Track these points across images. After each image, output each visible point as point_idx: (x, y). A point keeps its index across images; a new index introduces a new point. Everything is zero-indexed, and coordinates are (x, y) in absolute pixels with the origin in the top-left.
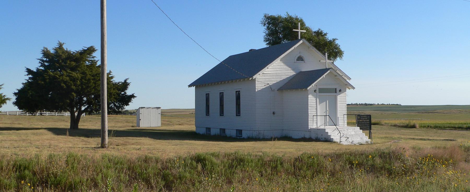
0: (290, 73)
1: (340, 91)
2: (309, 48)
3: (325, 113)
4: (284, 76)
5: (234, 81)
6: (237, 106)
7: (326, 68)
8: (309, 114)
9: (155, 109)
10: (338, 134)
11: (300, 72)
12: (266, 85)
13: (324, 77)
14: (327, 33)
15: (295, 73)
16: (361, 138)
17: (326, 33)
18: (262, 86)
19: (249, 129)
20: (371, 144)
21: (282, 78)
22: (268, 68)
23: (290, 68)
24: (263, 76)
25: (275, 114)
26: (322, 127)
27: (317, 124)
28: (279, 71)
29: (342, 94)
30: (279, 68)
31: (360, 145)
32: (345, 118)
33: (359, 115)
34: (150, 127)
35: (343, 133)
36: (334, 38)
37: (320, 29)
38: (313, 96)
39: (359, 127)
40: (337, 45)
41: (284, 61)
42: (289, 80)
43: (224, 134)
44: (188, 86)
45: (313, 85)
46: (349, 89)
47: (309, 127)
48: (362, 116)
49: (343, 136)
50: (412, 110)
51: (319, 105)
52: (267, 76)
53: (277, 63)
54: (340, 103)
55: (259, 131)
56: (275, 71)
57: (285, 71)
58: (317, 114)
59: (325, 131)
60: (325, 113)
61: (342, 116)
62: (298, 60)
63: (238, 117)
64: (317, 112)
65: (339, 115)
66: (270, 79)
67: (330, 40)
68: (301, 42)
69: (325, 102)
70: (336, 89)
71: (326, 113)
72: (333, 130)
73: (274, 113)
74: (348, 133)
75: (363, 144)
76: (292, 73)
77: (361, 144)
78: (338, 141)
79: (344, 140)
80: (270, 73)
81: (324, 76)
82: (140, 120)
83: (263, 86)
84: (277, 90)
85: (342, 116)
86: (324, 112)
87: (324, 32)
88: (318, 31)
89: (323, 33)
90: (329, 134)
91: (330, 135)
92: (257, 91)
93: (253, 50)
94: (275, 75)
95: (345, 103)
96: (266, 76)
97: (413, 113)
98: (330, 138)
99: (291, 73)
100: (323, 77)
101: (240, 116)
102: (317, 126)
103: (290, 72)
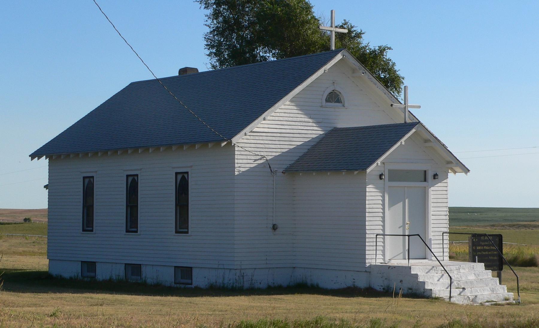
0: (310, 132)
1: (434, 178)
2: (354, 71)
3: (402, 228)
5: (174, 148)
6: (178, 208)
7: (405, 123)
8: (367, 232)
10: (438, 281)
11: (332, 130)
12: (258, 160)
13: (403, 143)
14: (363, 32)
15: (322, 133)
16: (493, 290)
17: (361, 31)
19: (216, 266)
20: (516, 304)
22: (264, 119)
24: (252, 137)
25: (277, 230)
26: (404, 263)
27: (384, 255)
29: (439, 184)
31: (492, 305)
32: (445, 242)
33: (474, 235)
36: (383, 44)
37: (347, 21)
39: (483, 264)
40: (388, 63)
41: (297, 102)
43: (140, 277)
44: (30, 156)
45: (379, 163)
46: (455, 172)
47: (367, 261)
50: (473, 220)
51: (389, 210)
53: (283, 107)
54: (435, 205)
57: (300, 128)
58: (384, 230)
59: (411, 272)
61: (437, 238)
62: (327, 101)
63: (182, 238)
64: (384, 226)
65: (432, 234)
66: (267, 146)
67: (373, 48)
68: (339, 57)
70: (425, 171)
71: (404, 230)
72: (427, 271)
73: (275, 227)
74: (461, 277)
75: (499, 305)
77: (496, 305)
78: (445, 294)
79: (456, 295)
80: (266, 130)
81: (403, 140)
83: (251, 161)
84: (282, 172)
85: (437, 238)
86: (399, 228)
87: (357, 29)
89: (355, 31)
90: (421, 279)
92: (238, 173)
93: (189, 73)
94: (279, 135)
95: (445, 205)
96: (257, 138)
97: (479, 227)
98: (424, 289)
99: (314, 132)
101: (187, 232)
102: (384, 259)
103: (312, 128)
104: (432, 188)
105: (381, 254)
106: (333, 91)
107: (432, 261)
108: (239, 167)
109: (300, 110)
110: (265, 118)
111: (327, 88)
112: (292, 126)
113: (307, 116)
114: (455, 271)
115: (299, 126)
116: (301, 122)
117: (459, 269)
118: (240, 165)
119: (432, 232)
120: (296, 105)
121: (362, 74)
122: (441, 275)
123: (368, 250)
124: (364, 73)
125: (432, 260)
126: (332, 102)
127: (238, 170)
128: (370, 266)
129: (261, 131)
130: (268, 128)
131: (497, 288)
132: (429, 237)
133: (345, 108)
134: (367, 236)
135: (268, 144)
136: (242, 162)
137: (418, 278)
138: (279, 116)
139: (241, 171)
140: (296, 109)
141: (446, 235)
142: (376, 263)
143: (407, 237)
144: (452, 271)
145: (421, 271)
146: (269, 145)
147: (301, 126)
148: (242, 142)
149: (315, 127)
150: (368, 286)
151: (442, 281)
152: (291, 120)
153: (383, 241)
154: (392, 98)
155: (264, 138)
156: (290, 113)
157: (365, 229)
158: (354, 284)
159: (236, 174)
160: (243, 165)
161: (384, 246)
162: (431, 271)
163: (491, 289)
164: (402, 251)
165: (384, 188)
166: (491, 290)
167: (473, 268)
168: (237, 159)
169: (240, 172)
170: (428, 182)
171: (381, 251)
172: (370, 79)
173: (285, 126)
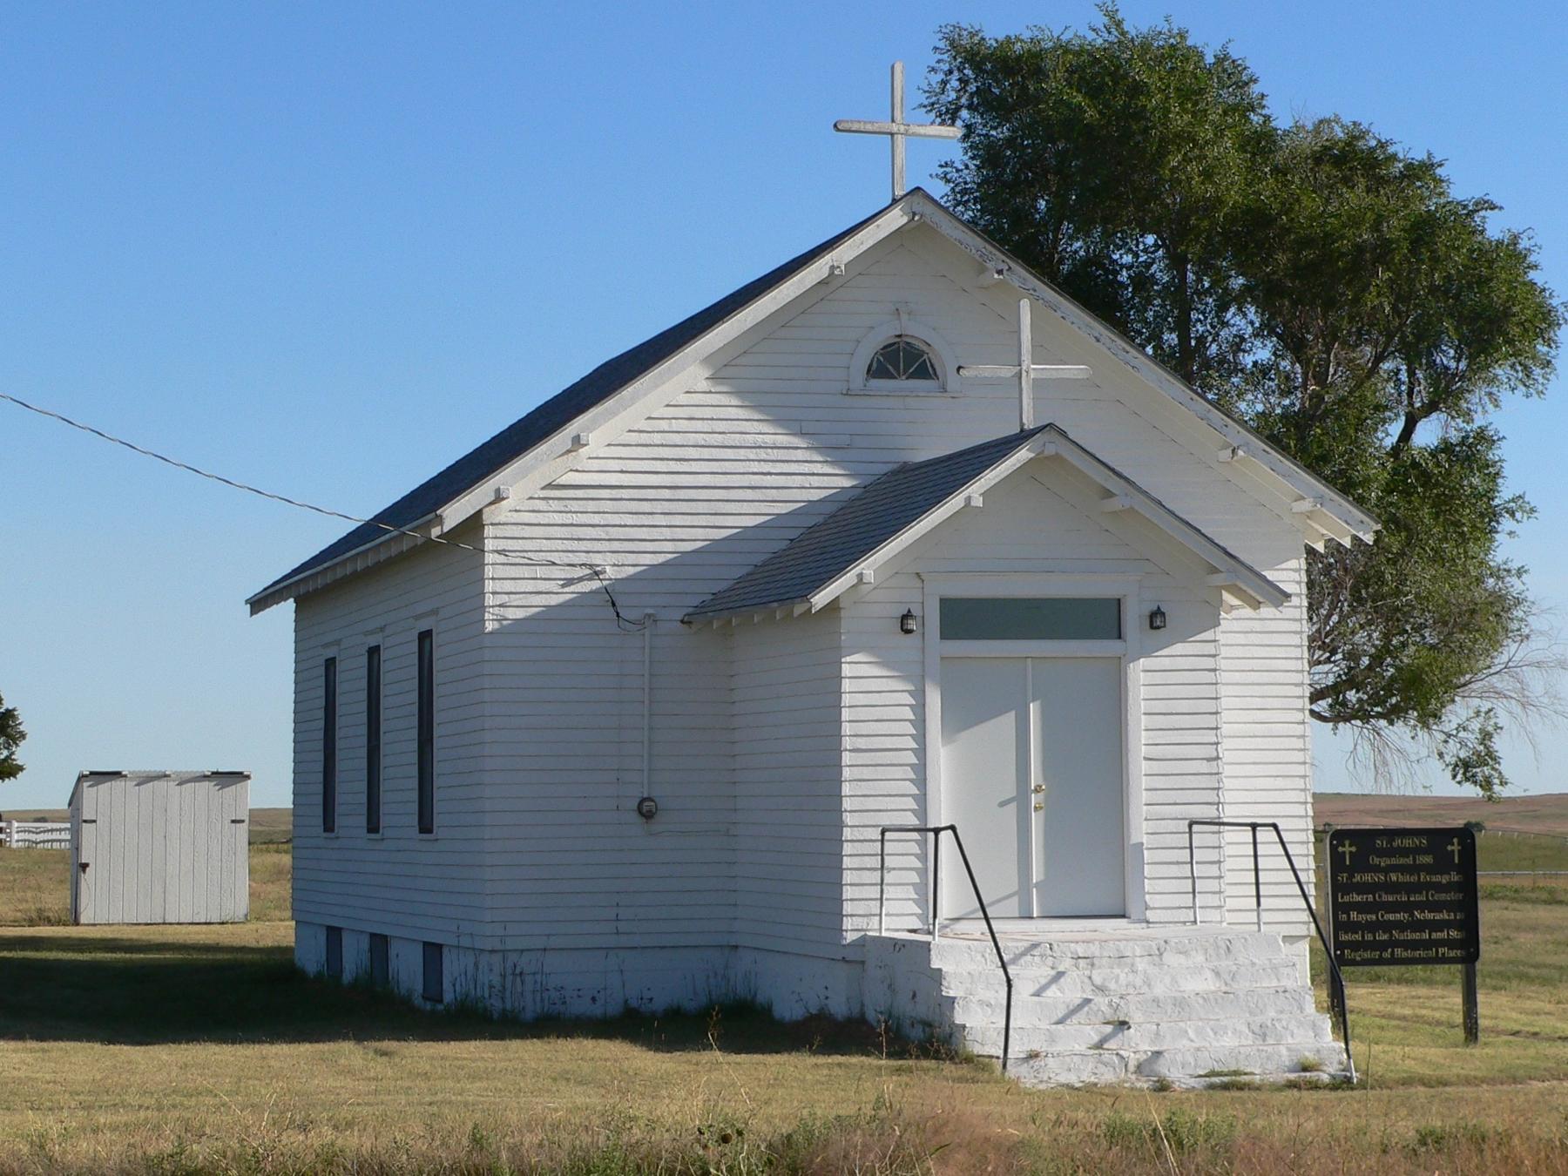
0: (798, 481)
3: (1013, 806)
4: (745, 508)
8: (848, 819)
9: (206, 784)
10: (1037, 994)
11: (894, 473)
12: (580, 579)
13: (978, 502)
15: (847, 483)
16: (1262, 1034)
18: (542, 586)
21: (730, 521)
23: (796, 441)
24: (555, 505)
28: (695, 467)
29: (1179, 648)
30: (700, 439)
31: (1212, 1087)
34: (161, 921)
35: (1098, 980)
42: (794, 534)
47: (848, 923)
49: (1079, 1007)
52: (591, 506)
55: (513, 957)
56: (659, 466)
57: (755, 467)
58: (922, 812)
60: (1013, 806)
69: (1013, 714)
70: (1119, 600)
76: (825, 481)
82: (84, 866)
83: (552, 586)
84: (682, 622)
86: (1002, 804)
88: (1349, 144)
91: (952, 994)
92: (497, 625)
94: (667, 494)
96: (575, 506)
99: (815, 481)
100: (969, 499)
103: (806, 468)
104: (1142, 660)
106: (898, 340)
107: (1144, 925)
108: (500, 606)
110: (579, 436)
111: (873, 328)
112: (727, 463)
113: (784, 427)
114: (1138, 959)
115: (753, 460)
116: (760, 447)
117: (1161, 954)
118: (507, 600)
119: (1146, 819)
121: (996, 276)
122: (1053, 973)
123: (851, 885)
124: (1005, 272)
125: (1148, 922)
126: (895, 378)
128: (863, 942)
129: (593, 484)
130: (622, 472)
131: (1284, 1023)
132: (1132, 837)
134: (847, 833)
135: (620, 526)
137: (944, 983)
138: (667, 429)
140: (740, 404)
141: (1214, 833)
142: (880, 929)
143: (931, 835)
144: (1128, 961)
145: (979, 957)
146: (627, 529)
147: (759, 461)
149: (819, 465)
150: (856, 1011)
151: (1059, 994)
152: (716, 444)
155: (608, 506)
156: (712, 419)
157: (840, 812)
158: (826, 1005)
159: (487, 631)
160: (515, 600)
162: (1029, 958)
163: (1257, 1029)
165: (923, 662)
166: (1254, 1033)
167: (1228, 948)
168: (493, 579)
169: (505, 622)
170: (1125, 641)
172: (1031, 292)
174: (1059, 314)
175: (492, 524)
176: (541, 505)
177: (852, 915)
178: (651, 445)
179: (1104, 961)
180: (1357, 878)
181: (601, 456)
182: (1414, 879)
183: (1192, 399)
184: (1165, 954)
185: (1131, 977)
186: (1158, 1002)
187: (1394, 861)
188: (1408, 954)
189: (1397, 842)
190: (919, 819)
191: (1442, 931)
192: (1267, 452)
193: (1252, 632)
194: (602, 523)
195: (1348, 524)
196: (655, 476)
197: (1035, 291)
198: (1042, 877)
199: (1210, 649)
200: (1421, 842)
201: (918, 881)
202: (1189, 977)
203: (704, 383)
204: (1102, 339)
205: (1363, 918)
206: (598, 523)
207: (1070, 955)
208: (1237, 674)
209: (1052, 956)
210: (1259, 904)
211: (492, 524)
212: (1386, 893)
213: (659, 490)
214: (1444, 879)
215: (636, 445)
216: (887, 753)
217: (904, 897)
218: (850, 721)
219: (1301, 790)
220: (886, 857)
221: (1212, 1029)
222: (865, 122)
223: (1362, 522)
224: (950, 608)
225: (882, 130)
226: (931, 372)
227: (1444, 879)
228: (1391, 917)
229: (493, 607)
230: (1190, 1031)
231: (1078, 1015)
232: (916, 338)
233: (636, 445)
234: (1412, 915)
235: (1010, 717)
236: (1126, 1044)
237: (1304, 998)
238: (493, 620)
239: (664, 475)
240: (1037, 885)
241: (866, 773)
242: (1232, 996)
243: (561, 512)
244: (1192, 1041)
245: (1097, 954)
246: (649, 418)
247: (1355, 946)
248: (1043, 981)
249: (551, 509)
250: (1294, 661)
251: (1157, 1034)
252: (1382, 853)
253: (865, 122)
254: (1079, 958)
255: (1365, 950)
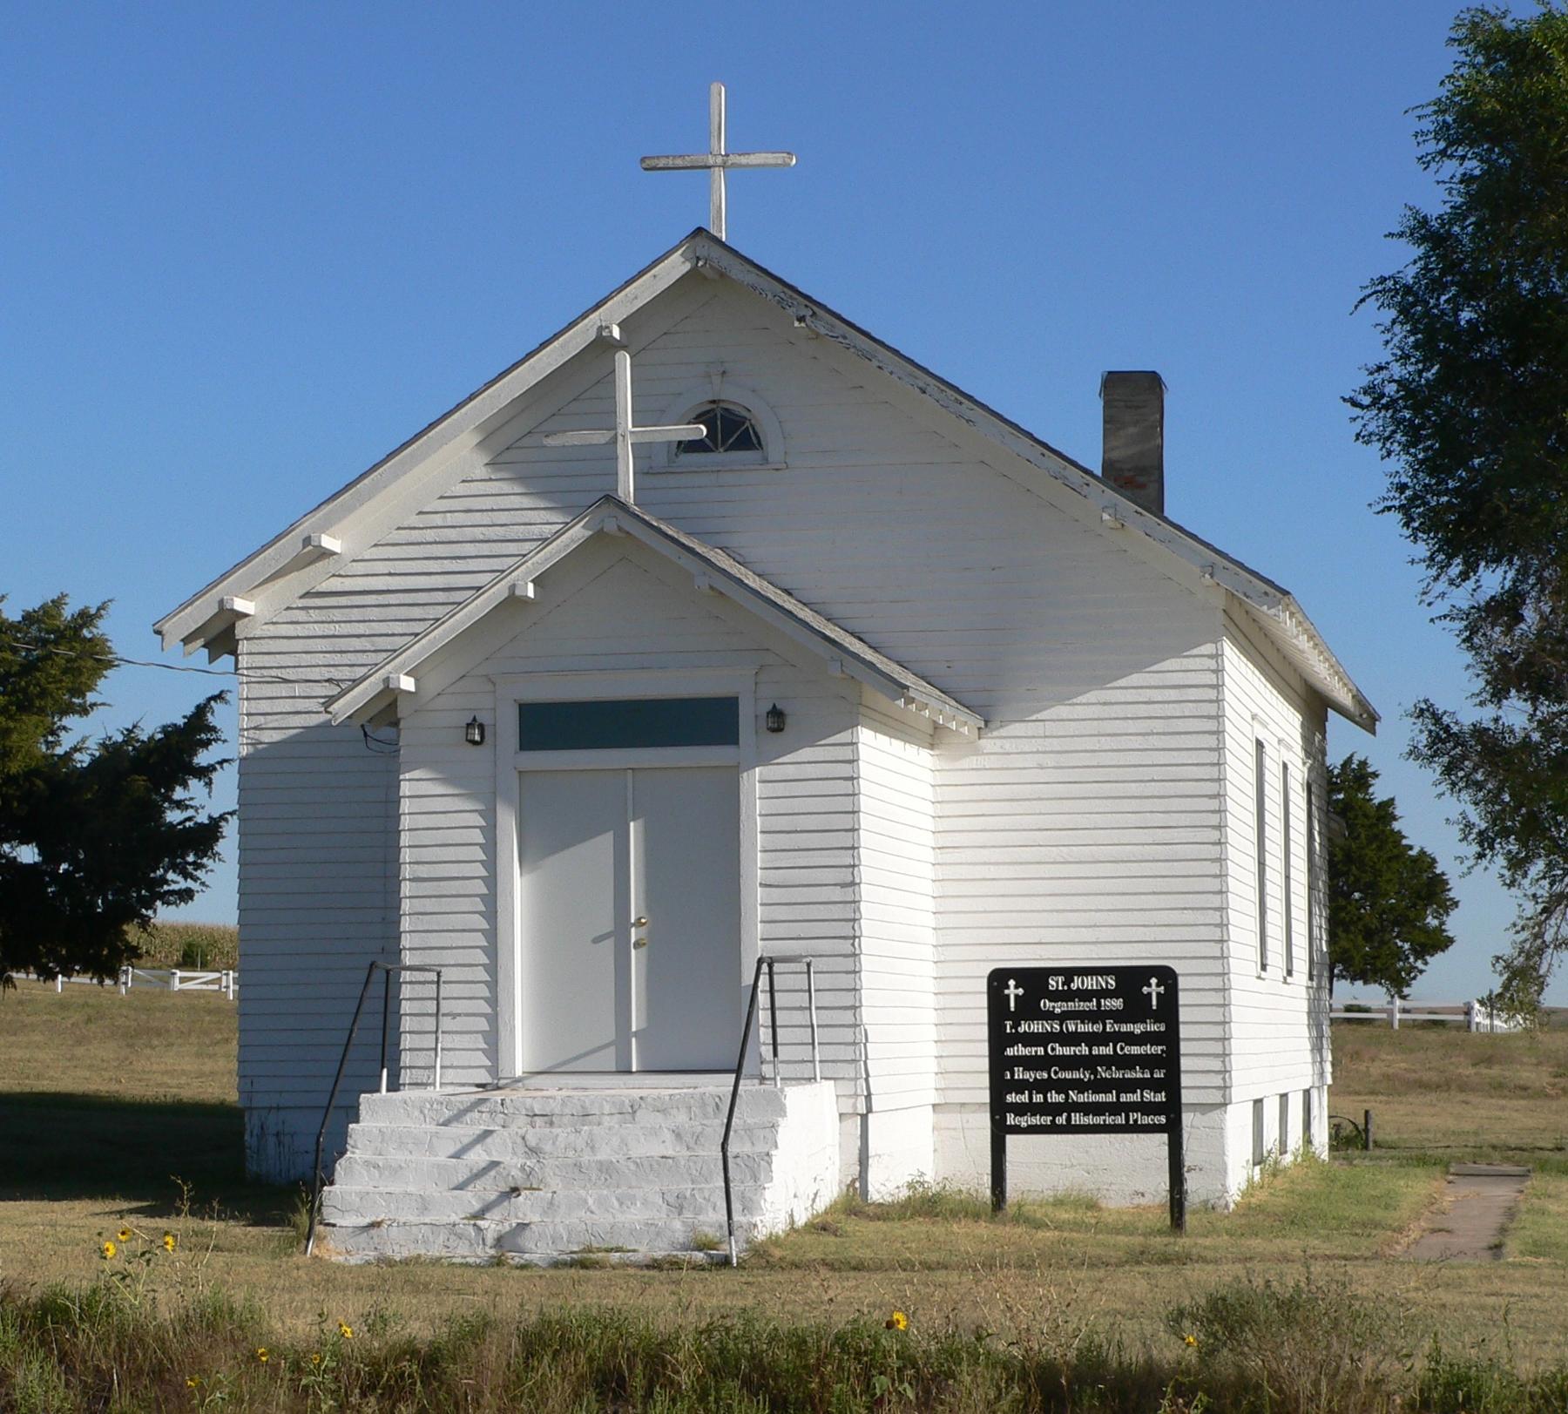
10: (457, 1156)
24: (314, 615)
29: (806, 753)
30: (478, 533)
35: (532, 1142)
38: (445, 781)
48: (1055, 983)
52: (356, 614)
60: (609, 944)
72: (447, 1114)
83: (313, 705)
86: (596, 940)
92: (251, 749)
96: (337, 615)
104: (757, 769)
105: (483, 1050)
106: (714, 406)
108: (255, 728)
109: (537, 493)
110: (310, 537)
117: (634, 1112)
120: (520, 478)
121: (796, 324)
123: (409, 1032)
124: (808, 318)
127: (249, 741)
130: (390, 574)
133: (769, 467)
136: (269, 711)
137: (349, 1140)
138: (440, 524)
139: (261, 743)
140: (523, 491)
145: (417, 1113)
148: (269, 634)
153: (487, 994)
154: (961, 403)
156: (492, 510)
160: (271, 721)
161: (496, 1015)
162: (476, 1114)
164: (610, 1034)
169: (260, 746)
171: (480, 1035)
172: (840, 339)
173: (468, 560)
174: (875, 363)
175: (246, 639)
176: (300, 616)
177: (410, 1067)
178: (422, 543)
179: (565, 1120)
180: (1023, 1028)
181: (366, 557)
182: (1098, 1028)
183: (1043, 455)
184: (638, 1114)
185: (572, 1137)
186: (581, 1167)
187: (1071, 1006)
188: (1090, 1120)
189: (1077, 983)
190: (489, 958)
191: (1134, 1092)
192: (1141, 514)
193: (1153, 734)
194: (367, 633)
195: (1247, 597)
196: (427, 578)
197: (845, 338)
198: (644, 1025)
199: (845, 753)
200: (1107, 983)
201: (488, 1029)
202: (642, 1140)
203: (484, 469)
204: (929, 390)
205: (1029, 1076)
206: (363, 632)
207: (524, 1112)
208: (1133, 785)
209: (503, 1113)
210: (775, 1054)
211: (246, 639)
212: (1061, 1045)
213: (432, 593)
214: (1138, 1029)
215: (406, 544)
216: (452, 883)
217: (471, 1046)
218: (409, 847)
219: (1216, 925)
220: (442, 1002)
221: (618, 1199)
222: (674, 157)
223: (1266, 594)
224: (528, 713)
225: (696, 164)
226: (755, 441)
227: (1138, 1029)
228: (1068, 1075)
229: (247, 729)
230: (590, 1201)
231: (483, 1179)
232: (735, 403)
233: (406, 544)
234: (1095, 1072)
235: (606, 841)
236: (512, 1213)
237: (759, 1166)
238: (247, 744)
239: (437, 576)
240: (636, 1034)
241: (429, 905)
242: (670, 1161)
243: (323, 622)
244: (592, 1212)
245: (557, 1111)
246: (421, 513)
247: (1020, 1109)
248: (466, 1141)
249: (312, 620)
250: (1208, 768)
251: (551, 1203)
252: (1056, 996)
253: (674, 157)
254: (536, 1115)
255: (1034, 1115)
